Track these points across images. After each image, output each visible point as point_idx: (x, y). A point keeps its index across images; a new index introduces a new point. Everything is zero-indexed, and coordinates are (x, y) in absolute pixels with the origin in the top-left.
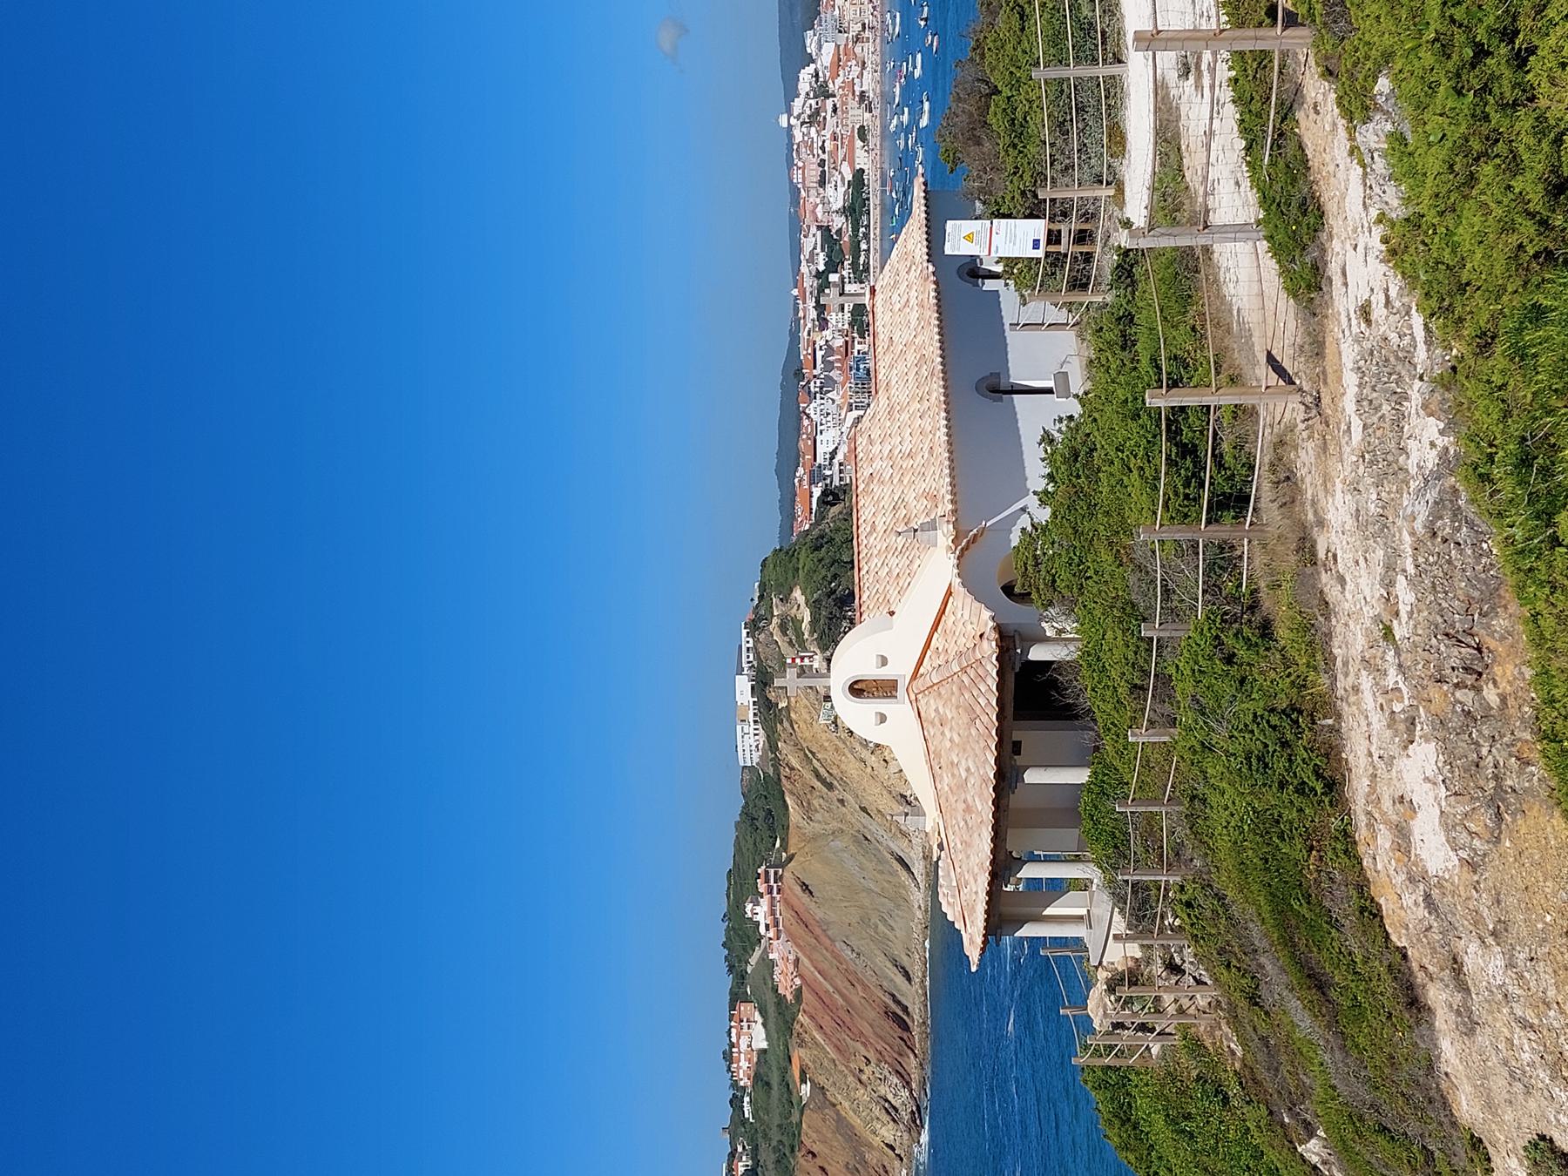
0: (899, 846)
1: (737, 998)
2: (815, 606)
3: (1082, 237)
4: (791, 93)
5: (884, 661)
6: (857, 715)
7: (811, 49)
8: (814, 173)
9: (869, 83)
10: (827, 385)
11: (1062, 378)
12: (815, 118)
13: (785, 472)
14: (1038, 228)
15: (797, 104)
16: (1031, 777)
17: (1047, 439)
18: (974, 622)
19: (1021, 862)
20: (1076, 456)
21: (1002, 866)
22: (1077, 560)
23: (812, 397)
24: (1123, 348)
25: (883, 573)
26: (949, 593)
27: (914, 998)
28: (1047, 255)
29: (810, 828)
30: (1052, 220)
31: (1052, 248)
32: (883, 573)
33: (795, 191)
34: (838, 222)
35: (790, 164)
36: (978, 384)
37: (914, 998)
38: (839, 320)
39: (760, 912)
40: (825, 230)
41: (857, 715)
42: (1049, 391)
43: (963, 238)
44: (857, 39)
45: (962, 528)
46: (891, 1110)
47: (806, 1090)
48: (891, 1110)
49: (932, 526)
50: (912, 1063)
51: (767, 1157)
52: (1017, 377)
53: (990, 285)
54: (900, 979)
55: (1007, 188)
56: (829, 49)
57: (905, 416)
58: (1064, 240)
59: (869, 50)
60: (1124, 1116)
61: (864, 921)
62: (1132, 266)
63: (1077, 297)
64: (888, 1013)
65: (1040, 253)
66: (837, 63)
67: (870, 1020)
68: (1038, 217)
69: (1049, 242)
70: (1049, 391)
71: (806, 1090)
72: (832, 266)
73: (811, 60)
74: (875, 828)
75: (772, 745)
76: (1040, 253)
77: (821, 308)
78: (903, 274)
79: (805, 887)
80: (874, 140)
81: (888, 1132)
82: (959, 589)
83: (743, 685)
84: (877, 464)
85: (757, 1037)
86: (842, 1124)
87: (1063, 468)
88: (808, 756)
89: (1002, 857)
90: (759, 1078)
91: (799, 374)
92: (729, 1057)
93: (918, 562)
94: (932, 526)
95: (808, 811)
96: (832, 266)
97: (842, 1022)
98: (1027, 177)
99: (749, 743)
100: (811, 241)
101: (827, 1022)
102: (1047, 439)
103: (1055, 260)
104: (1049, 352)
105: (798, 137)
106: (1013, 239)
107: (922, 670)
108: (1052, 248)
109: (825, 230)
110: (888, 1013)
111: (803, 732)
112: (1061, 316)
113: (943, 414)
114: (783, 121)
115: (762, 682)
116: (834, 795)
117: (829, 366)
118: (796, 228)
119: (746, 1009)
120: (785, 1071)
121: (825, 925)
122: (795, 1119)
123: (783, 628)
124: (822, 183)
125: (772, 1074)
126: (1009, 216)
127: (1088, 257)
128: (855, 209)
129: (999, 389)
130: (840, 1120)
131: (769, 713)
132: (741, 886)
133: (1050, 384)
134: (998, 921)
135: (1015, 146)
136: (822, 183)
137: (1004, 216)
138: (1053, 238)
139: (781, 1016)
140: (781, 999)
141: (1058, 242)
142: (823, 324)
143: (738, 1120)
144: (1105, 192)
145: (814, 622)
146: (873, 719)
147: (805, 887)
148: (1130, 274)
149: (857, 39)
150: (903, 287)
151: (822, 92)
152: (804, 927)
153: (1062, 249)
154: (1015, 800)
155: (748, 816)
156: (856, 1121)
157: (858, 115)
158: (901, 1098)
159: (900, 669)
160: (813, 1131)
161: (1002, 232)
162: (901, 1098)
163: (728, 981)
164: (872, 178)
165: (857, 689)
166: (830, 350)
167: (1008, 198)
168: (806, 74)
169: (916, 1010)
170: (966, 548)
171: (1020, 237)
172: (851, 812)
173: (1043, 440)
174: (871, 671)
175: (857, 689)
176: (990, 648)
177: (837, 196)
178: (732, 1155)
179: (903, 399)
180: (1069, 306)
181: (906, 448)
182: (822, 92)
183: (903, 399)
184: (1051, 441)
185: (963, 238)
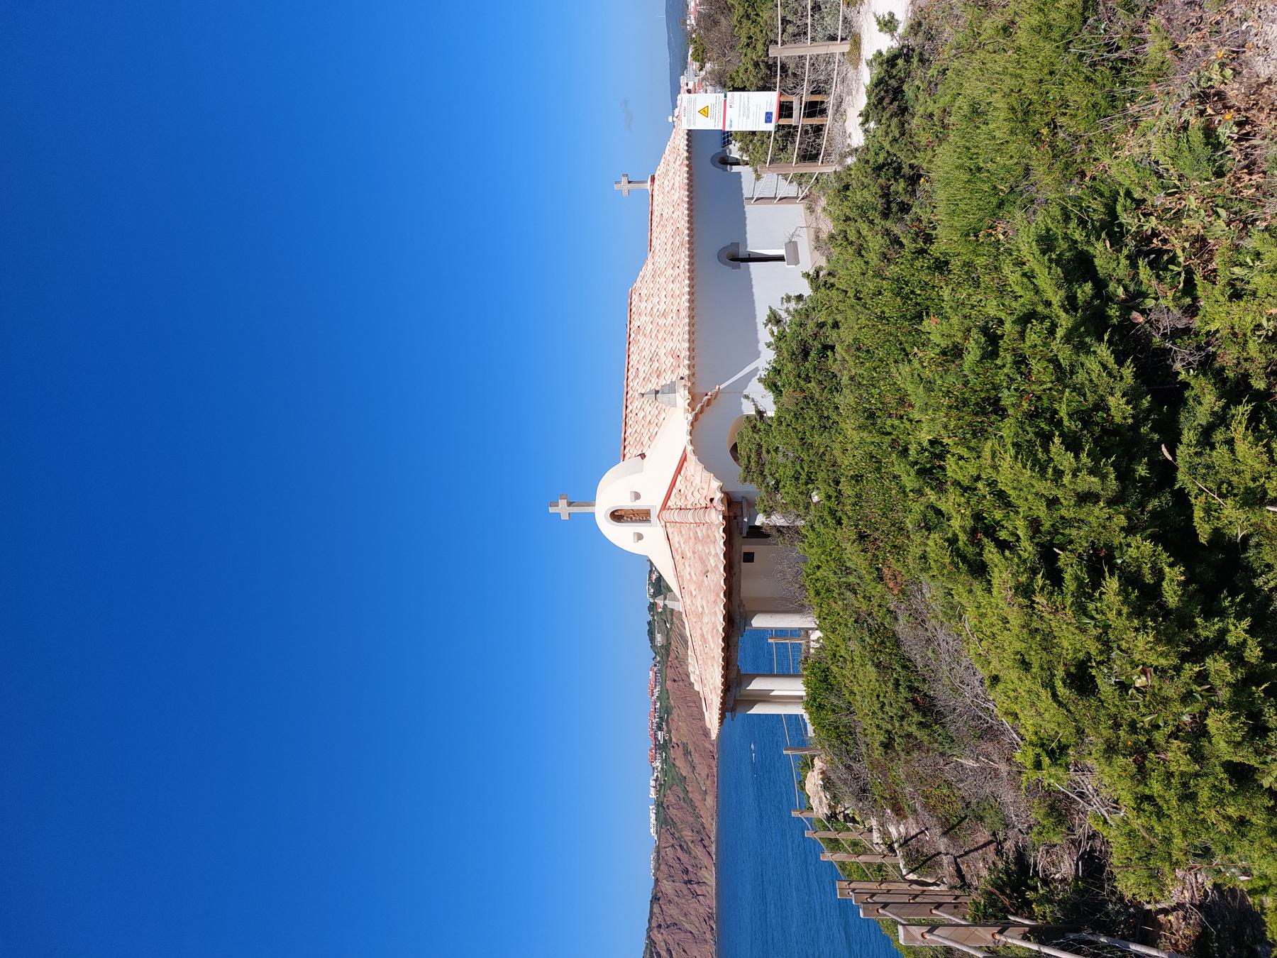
3: (814, 109)
5: (637, 496)
6: (621, 535)
11: (792, 245)
14: (769, 101)
16: (759, 622)
17: (775, 319)
18: (705, 486)
19: (753, 677)
20: (806, 354)
22: (804, 476)
24: (886, 215)
25: (641, 414)
26: (684, 459)
28: (779, 127)
30: (784, 91)
31: (783, 122)
32: (641, 414)
36: (722, 254)
41: (621, 535)
42: (781, 259)
45: (699, 390)
49: (671, 388)
52: (754, 247)
53: (735, 169)
55: (741, 62)
57: (663, 279)
58: (795, 113)
62: (902, 81)
63: (807, 168)
65: (771, 127)
68: (769, 89)
69: (780, 116)
70: (781, 259)
76: (771, 127)
78: (671, 164)
82: (692, 458)
84: (643, 318)
87: (790, 366)
89: (733, 675)
93: (663, 415)
94: (671, 388)
98: (760, 46)
102: (775, 319)
103: (786, 133)
104: (786, 226)
106: (746, 112)
107: (669, 503)
108: (783, 122)
112: (791, 190)
113: (687, 282)
114: (670, 119)
126: (744, 89)
127: (818, 130)
129: (739, 258)
133: (782, 252)
135: (748, 17)
137: (736, 89)
138: (785, 110)
141: (790, 116)
144: (840, 48)
146: (631, 537)
148: (898, 93)
150: (671, 174)
153: (793, 122)
154: (744, 643)
159: (651, 500)
161: (736, 105)
165: (617, 516)
167: (742, 71)
170: (701, 406)
171: (753, 111)
173: (769, 320)
174: (626, 503)
175: (617, 516)
176: (716, 518)
179: (663, 265)
180: (800, 179)
181: (662, 307)
183: (663, 265)
184: (778, 321)
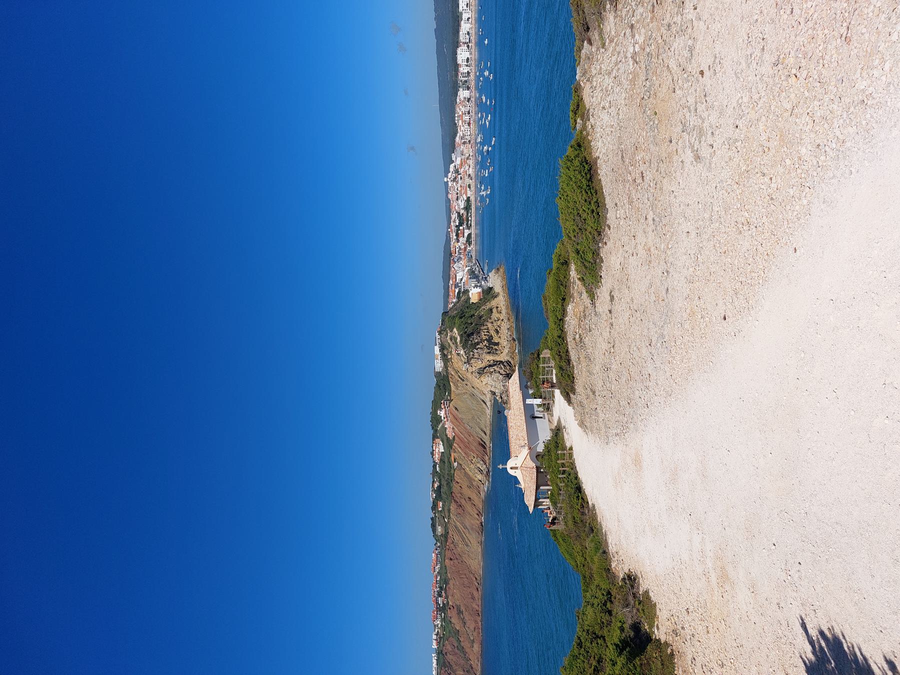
0: (483, 397)
1: (434, 437)
2: (461, 336)
4: (447, 171)
7: (454, 159)
8: (455, 196)
9: (471, 171)
10: (460, 258)
12: (455, 180)
13: (447, 288)
15: (450, 174)
21: (536, 500)
23: (455, 262)
27: (487, 439)
29: (457, 392)
33: (448, 201)
34: (462, 212)
35: (447, 193)
37: (487, 439)
38: (463, 240)
39: (442, 413)
40: (459, 213)
43: (529, 401)
44: (468, 158)
46: (481, 471)
47: (456, 464)
48: (481, 471)
50: (487, 458)
51: (444, 483)
54: (483, 434)
56: (459, 159)
59: (471, 162)
60: (555, 535)
61: (473, 418)
64: (480, 444)
66: (461, 164)
67: (474, 446)
71: (456, 464)
72: (461, 224)
73: (453, 162)
74: (476, 392)
75: (446, 366)
77: (457, 235)
79: (456, 409)
80: (473, 188)
81: (480, 477)
83: (437, 349)
85: (440, 448)
86: (466, 474)
88: (457, 372)
90: (441, 460)
91: (451, 255)
92: (432, 454)
95: (457, 387)
96: (461, 224)
97: (466, 446)
99: (439, 365)
100: (454, 216)
101: (462, 446)
105: (450, 184)
109: (459, 213)
110: (480, 444)
111: (455, 365)
115: (442, 348)
116: (465, 382)
117: (460, 254)
118: (449, 211)
119: (437, 440)
120: (449, 459)
121: (462, 419)
122: (452, 472)
123: (451, 339)
124: (457, 199)
125: (445, 459)
128: (467, 208)
130: (466, 473)
131: (444, 357)
132: (436, 406)
134: (536, 506)
136: (457, 199)
139: (449, 444)
140: (448, 438)
142: (458, 241)
143: (435, 472)
145: (461, 341)
147: (456, 409)
149: (468, 158)
151: (457, 171)
152: (456, 420)
155: (438, 385)
156: (470, 474)
157: (468, 181)
158: (483, 467)
159: (519, 465)
160: (458, 476)
162: (483, 467)
163: (432, 432)
164: (472, 199)
166: (460, 249)
168: (452, 166)
169: (488, 443)
172: (469, 387)
177: (462, 204)
178: (433, 481)
182: (457, 171)
185: (529, 401)
